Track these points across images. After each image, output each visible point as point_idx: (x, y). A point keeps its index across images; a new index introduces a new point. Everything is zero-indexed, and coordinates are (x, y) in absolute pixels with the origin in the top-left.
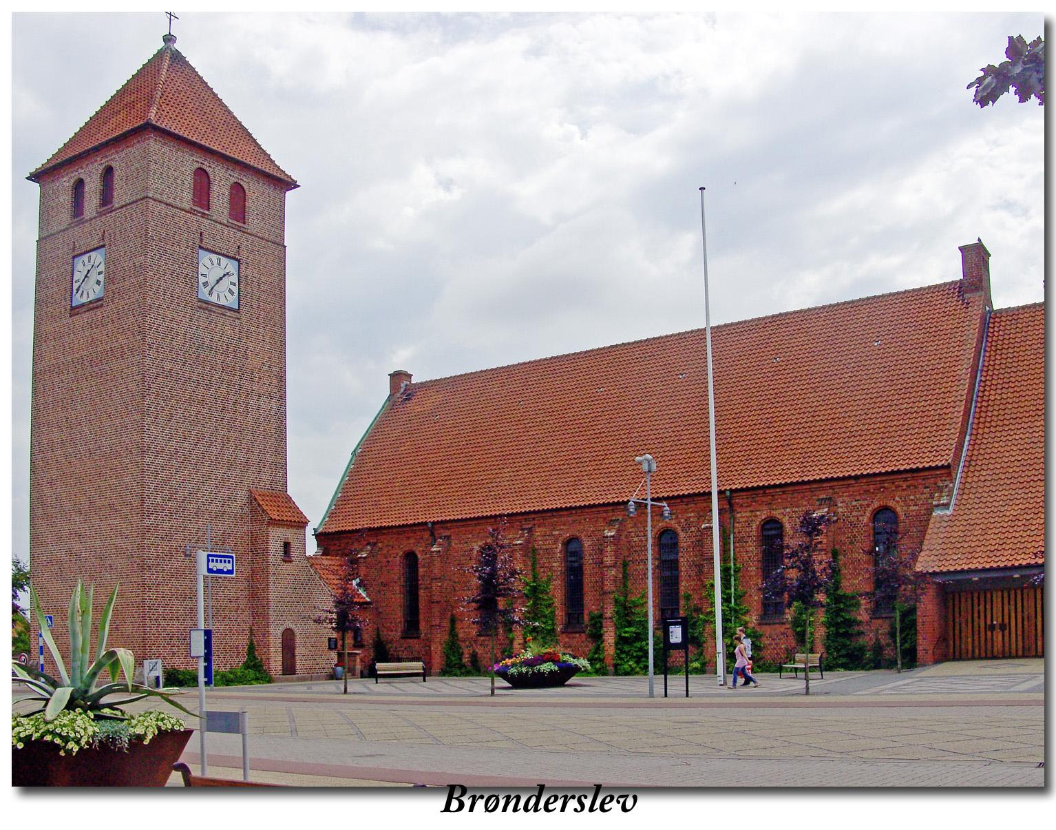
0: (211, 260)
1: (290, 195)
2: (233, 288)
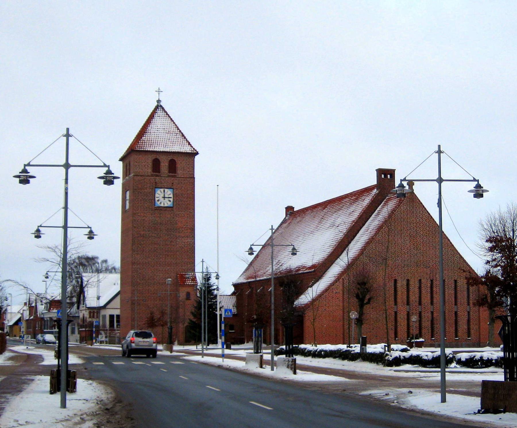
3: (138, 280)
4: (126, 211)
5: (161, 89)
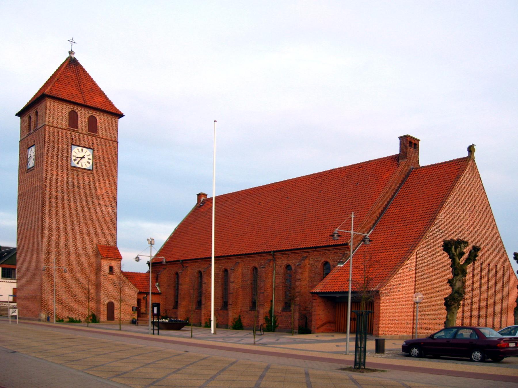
0: (78, 149)
1: (121, 120)
2: (89, 161)
3: (50, 248)
4: (29, 170)
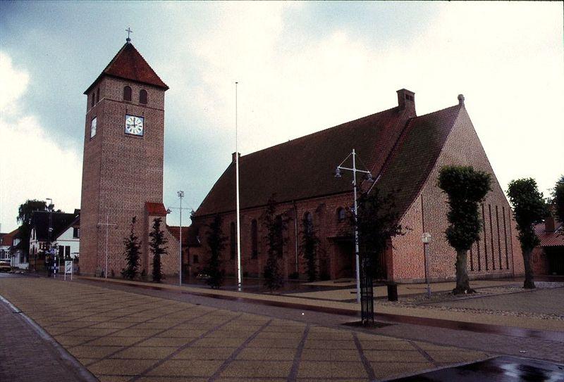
5: (131, 29)
